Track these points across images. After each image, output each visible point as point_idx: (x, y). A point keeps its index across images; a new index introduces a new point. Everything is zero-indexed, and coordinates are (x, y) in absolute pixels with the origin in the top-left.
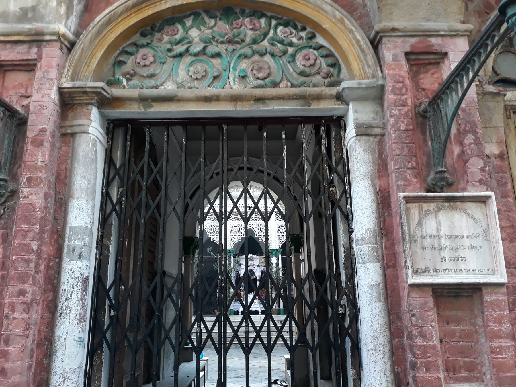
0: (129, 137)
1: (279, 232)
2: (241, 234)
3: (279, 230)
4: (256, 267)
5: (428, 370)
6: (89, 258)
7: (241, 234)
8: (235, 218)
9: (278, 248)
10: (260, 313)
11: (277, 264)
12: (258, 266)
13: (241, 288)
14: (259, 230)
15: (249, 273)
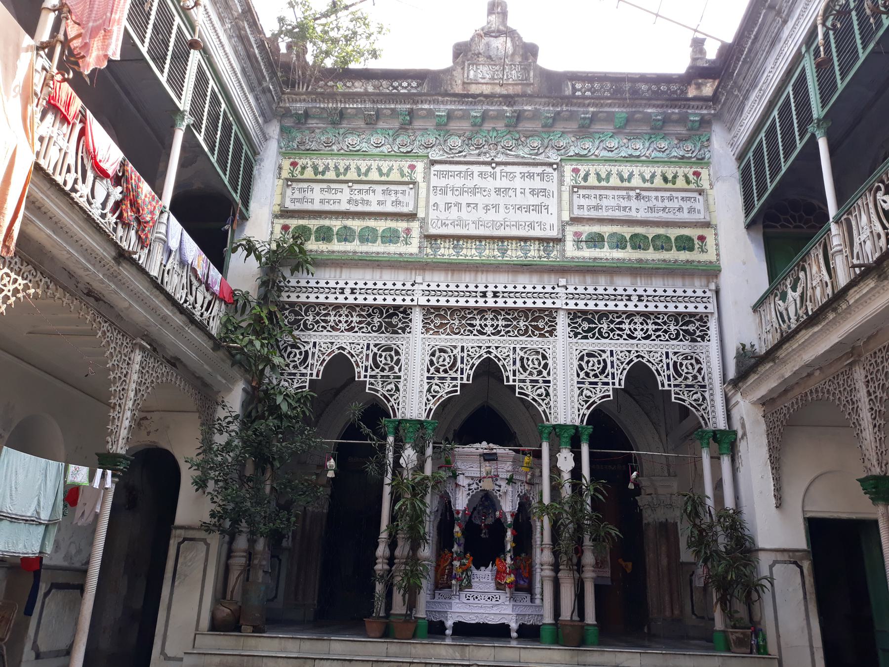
0: (117, 87)
1: (582, 374)
2: (458, 375)
3: (581, 368)
4: (503, 484)
5: (542, 179)
6: (321, 415)
7: (458, 375)
8: (442, 325)
9: (577, 422)
10: (514, 634)
11: (576, 472)
12: (510, 481)
13: (456, 548)
14: (518, 363)
15: (485, 501)
